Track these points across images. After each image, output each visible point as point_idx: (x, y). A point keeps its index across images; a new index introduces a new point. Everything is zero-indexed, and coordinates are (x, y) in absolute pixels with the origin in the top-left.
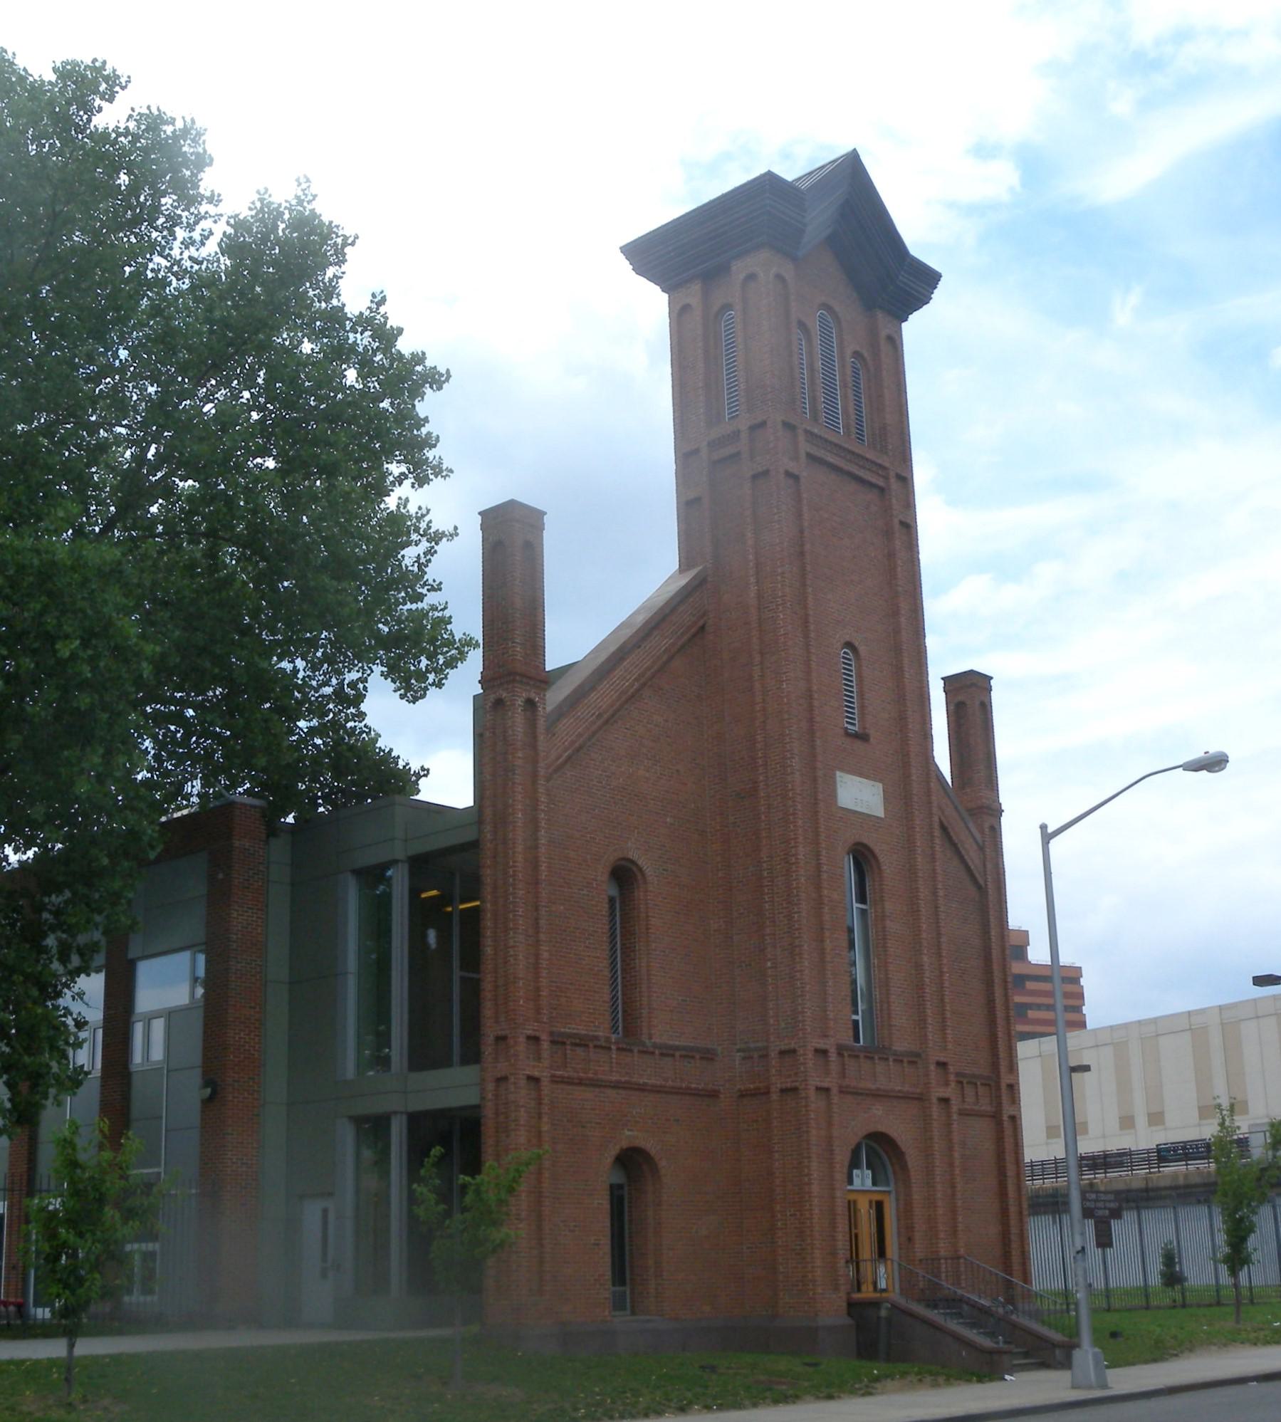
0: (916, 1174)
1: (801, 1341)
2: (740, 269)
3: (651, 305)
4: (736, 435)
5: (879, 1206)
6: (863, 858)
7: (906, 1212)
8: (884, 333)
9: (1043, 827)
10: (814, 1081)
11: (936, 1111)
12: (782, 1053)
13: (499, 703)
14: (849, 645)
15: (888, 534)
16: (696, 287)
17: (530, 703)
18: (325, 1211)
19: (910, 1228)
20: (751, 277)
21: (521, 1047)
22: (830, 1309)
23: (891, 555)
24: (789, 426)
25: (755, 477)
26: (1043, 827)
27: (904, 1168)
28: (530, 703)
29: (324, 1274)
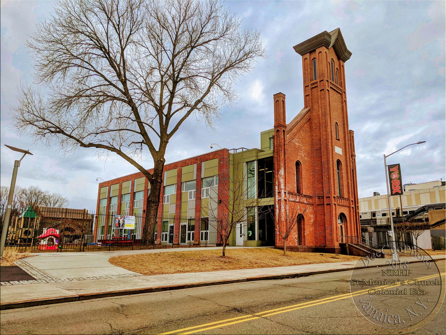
0: (348, 221)
1: (332, 251)
2: (318, 51)
3: (298, 60)
4: (317, 82)
5: (342, 226)
6: (339, 162)
7: (346, 227)
8: (341, 64)
9: (384, 155)
10: (333, 202)
11: (352, 209)
12: (327, 197)
13: (278, 131)
14: (336, 123)
15: (342, 103)
16: (308, 54)
17: (284, 131)
18: (241, 225)
19: (347, 231)
20: (320, 52)
21: (333, 199)
22: (337, 245)
23: (343, 107)
24: (327, 81)
25: (321, 90)
26: (384, 155)
27: (346, 220)
28: (284, 131)
29: (241, 236)
